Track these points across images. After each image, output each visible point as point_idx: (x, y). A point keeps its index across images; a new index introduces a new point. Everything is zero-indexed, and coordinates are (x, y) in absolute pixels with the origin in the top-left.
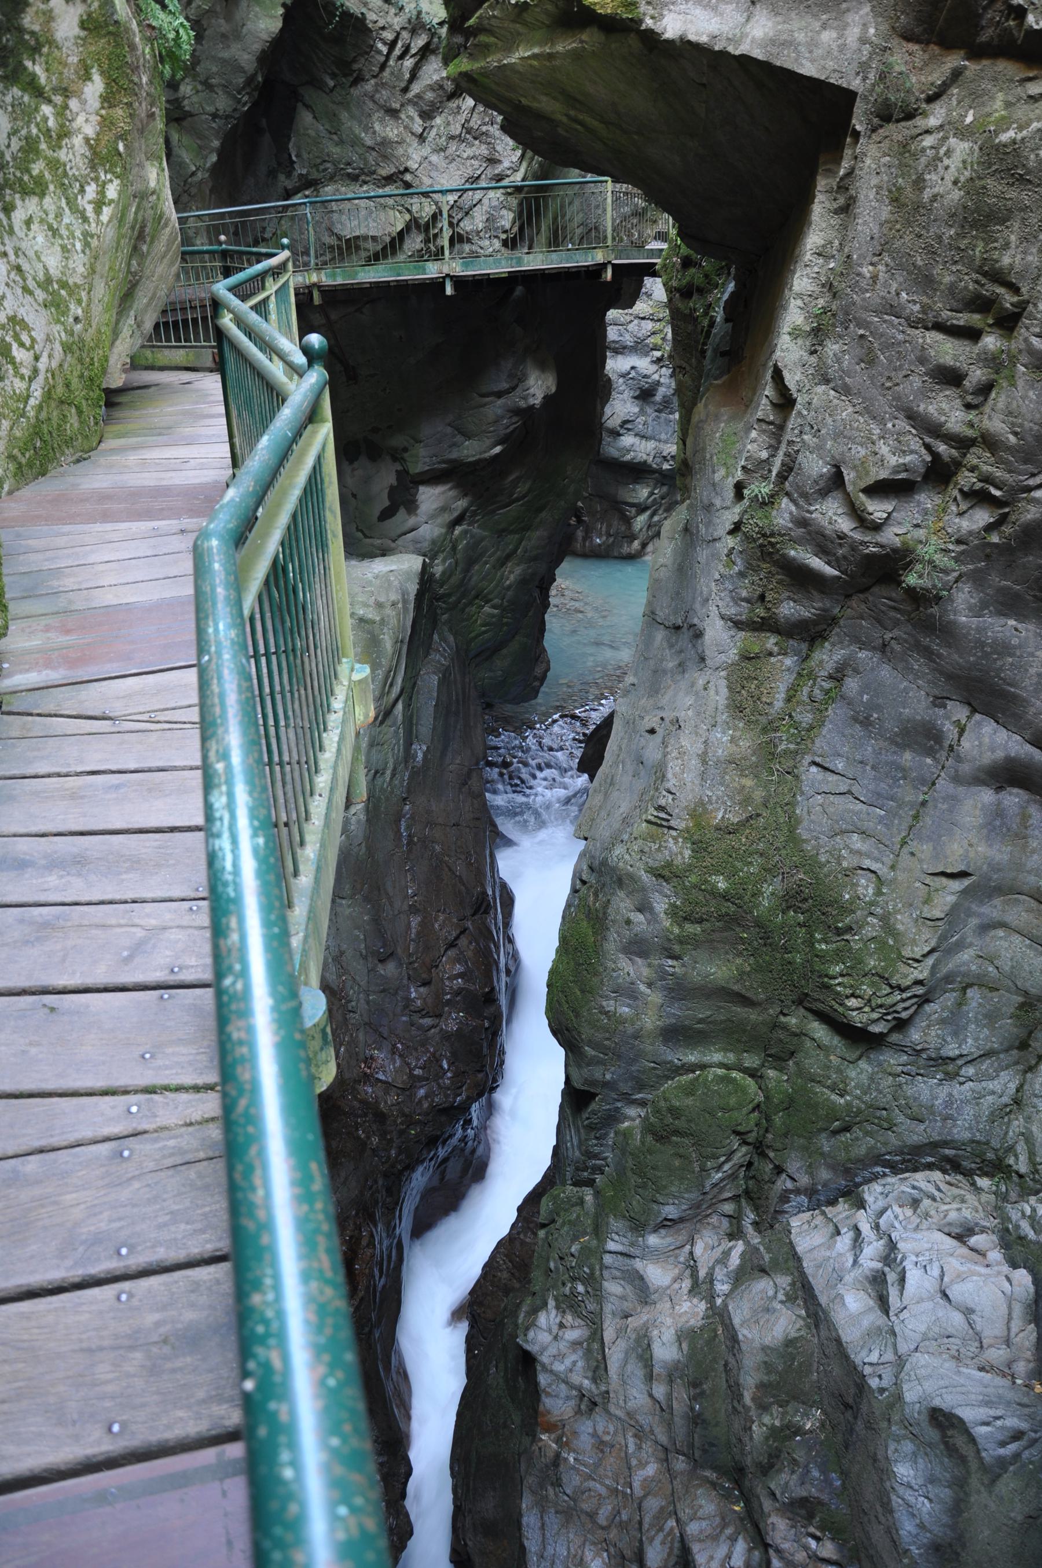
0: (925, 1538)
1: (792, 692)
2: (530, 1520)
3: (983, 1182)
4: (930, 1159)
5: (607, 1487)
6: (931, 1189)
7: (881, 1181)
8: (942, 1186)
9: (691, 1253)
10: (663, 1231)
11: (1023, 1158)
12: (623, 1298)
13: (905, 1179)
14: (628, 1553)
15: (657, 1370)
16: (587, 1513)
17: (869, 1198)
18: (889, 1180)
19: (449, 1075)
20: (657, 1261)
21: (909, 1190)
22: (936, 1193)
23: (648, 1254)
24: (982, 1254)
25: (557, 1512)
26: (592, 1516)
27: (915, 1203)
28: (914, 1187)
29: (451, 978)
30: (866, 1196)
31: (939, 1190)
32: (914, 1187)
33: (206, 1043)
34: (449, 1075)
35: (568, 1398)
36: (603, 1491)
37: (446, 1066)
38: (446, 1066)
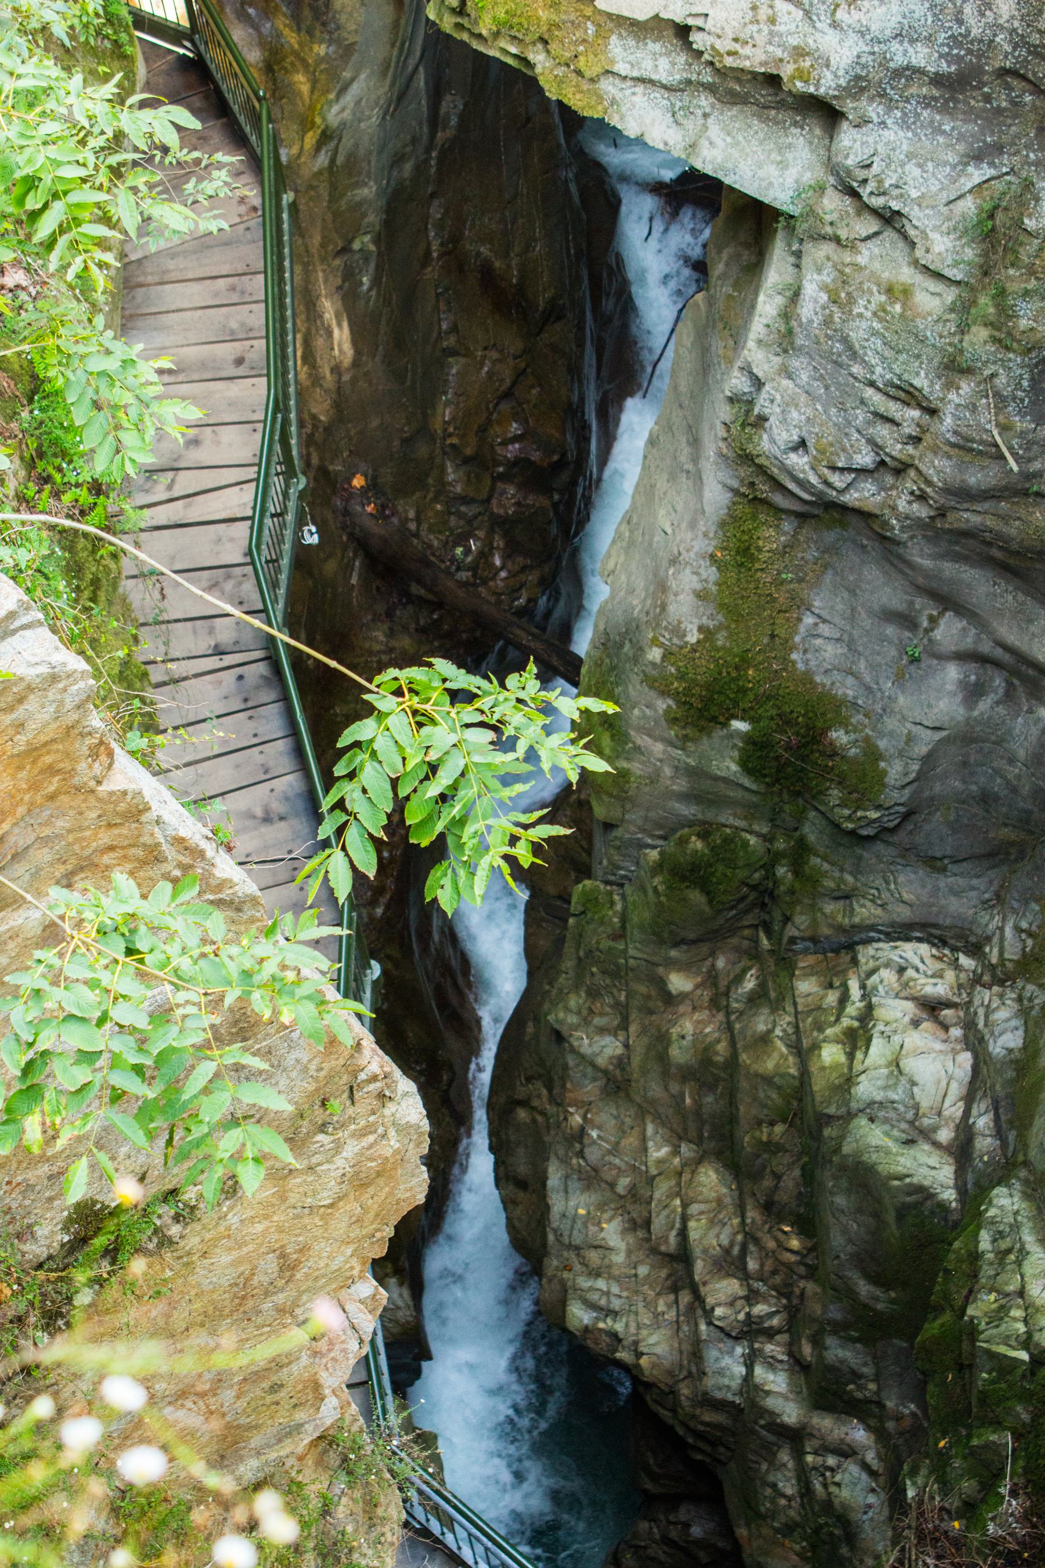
0: (850, 1248)
1: (333, 1459)
2: (554, 1179)
3: (965, 961)
4: (918, 934)
5: (627, 1163)
6: (917, 961)
7: (876, 945)
8: (928, 961)
9: (713, 965)
10: (685, 947)
11: (996, 951)
12: (648, 997)
13: (896, 947)
14: (639, 1221)
15: (673, 1070)
16: (607, 1182)
17: (862, 959)
18: (881, 945)
19: (503, 574)
20: (679, 970)
21: (897, 959)
22: (921, 966)
23: (672, 964)
24: (946, 1028)
25: (579, 1179)
26: (612, 1185)
27: (901, 970)
28: (901, 957)
29: (505, 443)
30: (860, 957)
31: (923, 962)
32: (901, 957)
33: (510, 1333)
34: (503, 574)
35: (594, 1079)
36: (623, 1166)
37: (498, 562)
38: (498, 562)
